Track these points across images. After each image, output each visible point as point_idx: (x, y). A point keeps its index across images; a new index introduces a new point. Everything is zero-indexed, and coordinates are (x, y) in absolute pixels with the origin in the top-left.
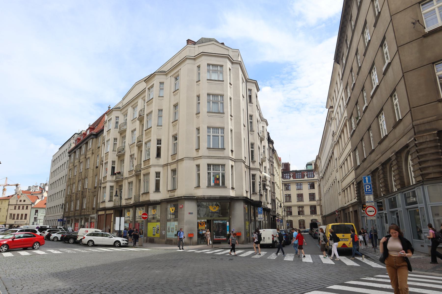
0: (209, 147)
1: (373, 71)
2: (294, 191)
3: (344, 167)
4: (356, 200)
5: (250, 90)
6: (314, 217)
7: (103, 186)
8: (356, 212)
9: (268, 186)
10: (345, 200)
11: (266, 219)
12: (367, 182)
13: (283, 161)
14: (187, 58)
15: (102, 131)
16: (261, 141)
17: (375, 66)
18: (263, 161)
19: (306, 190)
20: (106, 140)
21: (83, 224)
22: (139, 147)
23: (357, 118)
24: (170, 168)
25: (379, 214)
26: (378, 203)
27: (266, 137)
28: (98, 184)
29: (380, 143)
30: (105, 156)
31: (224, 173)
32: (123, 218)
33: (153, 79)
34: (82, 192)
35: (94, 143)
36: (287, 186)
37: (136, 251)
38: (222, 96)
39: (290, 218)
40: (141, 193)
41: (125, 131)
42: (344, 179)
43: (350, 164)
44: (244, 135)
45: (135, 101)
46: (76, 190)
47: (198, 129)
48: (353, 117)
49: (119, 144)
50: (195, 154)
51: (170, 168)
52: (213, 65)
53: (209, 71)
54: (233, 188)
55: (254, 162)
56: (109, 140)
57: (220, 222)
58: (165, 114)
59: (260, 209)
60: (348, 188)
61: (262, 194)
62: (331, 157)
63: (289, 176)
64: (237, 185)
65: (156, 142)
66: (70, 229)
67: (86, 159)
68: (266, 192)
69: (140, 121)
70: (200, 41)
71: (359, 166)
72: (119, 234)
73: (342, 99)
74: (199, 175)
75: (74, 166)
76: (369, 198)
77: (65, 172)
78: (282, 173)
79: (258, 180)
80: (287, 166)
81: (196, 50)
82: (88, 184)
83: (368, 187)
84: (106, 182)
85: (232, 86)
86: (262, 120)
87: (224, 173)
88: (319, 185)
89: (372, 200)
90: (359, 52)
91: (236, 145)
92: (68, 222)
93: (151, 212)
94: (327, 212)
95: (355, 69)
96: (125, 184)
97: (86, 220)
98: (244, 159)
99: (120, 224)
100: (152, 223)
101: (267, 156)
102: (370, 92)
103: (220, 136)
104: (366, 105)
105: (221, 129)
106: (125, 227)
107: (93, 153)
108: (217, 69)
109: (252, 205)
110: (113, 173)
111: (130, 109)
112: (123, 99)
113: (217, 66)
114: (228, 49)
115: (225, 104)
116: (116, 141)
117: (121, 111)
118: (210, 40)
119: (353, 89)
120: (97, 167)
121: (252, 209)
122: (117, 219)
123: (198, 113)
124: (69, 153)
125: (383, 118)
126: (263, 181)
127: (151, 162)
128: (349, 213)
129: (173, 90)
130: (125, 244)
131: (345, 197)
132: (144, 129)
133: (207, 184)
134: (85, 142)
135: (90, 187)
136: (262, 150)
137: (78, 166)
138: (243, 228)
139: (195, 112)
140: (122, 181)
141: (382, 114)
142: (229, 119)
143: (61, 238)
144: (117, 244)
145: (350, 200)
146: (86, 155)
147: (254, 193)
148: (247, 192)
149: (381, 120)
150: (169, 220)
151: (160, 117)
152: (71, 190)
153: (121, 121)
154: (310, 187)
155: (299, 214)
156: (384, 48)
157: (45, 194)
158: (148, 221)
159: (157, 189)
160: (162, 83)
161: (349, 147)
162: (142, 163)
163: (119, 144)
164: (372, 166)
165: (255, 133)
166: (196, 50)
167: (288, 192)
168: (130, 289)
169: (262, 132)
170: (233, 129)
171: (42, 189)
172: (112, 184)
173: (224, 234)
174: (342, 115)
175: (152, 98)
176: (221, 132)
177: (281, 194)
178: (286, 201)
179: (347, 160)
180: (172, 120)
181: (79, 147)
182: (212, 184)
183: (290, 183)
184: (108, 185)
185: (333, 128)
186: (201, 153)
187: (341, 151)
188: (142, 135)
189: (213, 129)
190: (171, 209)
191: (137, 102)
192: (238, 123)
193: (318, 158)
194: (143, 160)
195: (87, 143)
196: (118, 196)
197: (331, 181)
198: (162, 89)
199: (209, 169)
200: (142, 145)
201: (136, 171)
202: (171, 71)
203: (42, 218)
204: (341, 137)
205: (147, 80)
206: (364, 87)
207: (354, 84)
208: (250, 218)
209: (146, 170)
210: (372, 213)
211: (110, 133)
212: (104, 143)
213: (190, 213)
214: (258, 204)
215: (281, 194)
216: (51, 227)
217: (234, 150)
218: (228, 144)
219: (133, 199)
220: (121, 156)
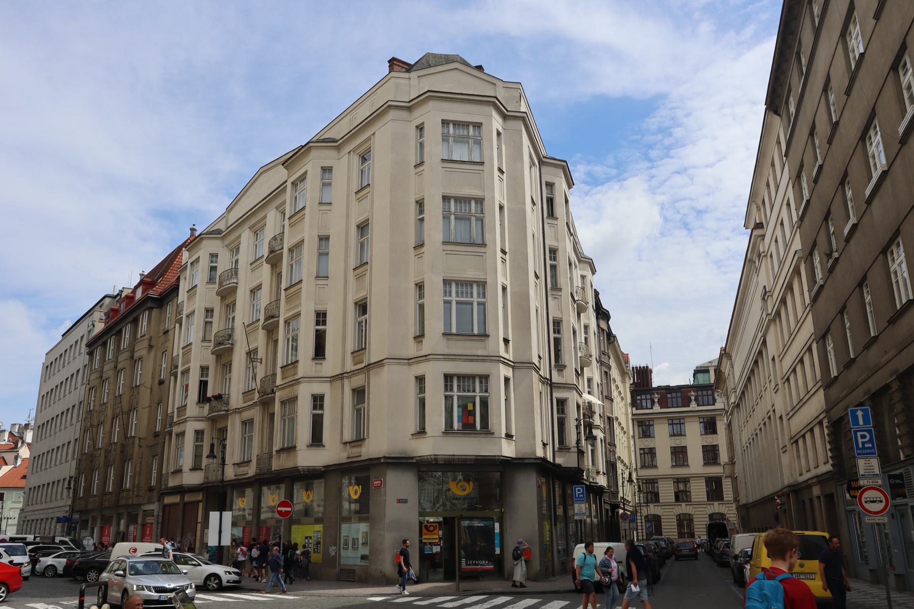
0: (448, 332)
1: (872, 132)
2: (662, 439)
3: (796, 379)
4: (829, 467)
5: (550, 185)
6: (717, 507)
7: (176, 429)
8: (830, 498)
9: (598, 427)
10: (800, 467)
11: (593, 514)
12: (861, 422)
13: (636, 361)
14: (390, 106)
16: (580, 310)
17: (876, 121)
18: (584, 363)
19: (694, 438)
20: (185, 313)
21: (122, 528)
22: (271, 330)
23: (829, 255)
25: (895, 506)
26: (890, 477)
28: (164, 426)
29: (892, 321)
30: (184, 355)
31: (487, 398)
32: (228, 516)
33: (305, 161)
34: (123, 446)
35: (153, 322)
36: (644, 427)
37: (262, 602)
38: (480, 201)
39: (653, 509)
40: (275, 449)
41: (234, 290)
42: (795, 410)
43: (811, 372)
44: (535, 300)
45: (260, 216)
46: (106, 441)
47: (420, 286)
48: (816, 252)
49: (217, 325)
50: (412, 350)
52: (457, 124)
53: (445, 138)
54: (509, 436)
55: (561, 367)
56: (193, 313)
57: (476, 524)
58: (335, 247)
59: (579, 490)
60: (808, 436)
61: (584, 449)
62: (760, 353)
64: (520, 429)
66: (89, 543)
67: (134, 361)
68: (593, 445)
69: (272, 267)
70: (424, 61)
71: (836, 378)
72: (218, 555)
73: (788, 204)
74: (422, 403)
75: (102, 380)
76: (868, 466)
77: (76, 395)
78: (632, 392)
79: (572, 414)
80: (644, 374)
81: (411, 86)
82: (138, 426)
83: (863, 437)
84: (185, 421)
85: (504, 177)
86: (579, 261)
87: (487, 398)
88: (729, 425)
89: (877, 471)
90: (833, 83)
91: (515, 329)
92: (84, 524)
93: (302, 497)
94: (751, 494)
95: (823, 128)
96: (233, 425)
97: (132, 519)
98: (535, 360)
99: (220, 528)
100: (300, 526)
101: (594, 352)
102: (864, 189)
103: (475, 304)
104: (853, 220)
105: (478, 286)
106: (233, 535)
107: (151, 347)
108: (466, 133)
109: (560, 479)
110: (203, 398)
111: (246, 236)
112: (230, 209)
113: (465, 125)
114: (493, 81)
115: (487, 221)
116: (212, 316)
117: (223, 238)
118: (448, 59)
119: (816, 181)
120: (161, 383)
121: (557, 486)
122: (214, 516)
123: (419, 246)
124: (89, 345)
125: (899, 256)
126: (584, 415)
128: (811, 500)
129: (355, 187)
130: (234, 582)
131: (799, 457)
132: (284, 286)
134: (131, 319)
135: (143, 433)
136: (581, 337)
138: (537, 539)
139: (412, 242)
140: (225, 417)
141: (898, 245)
142: (499, 260)
143: (66, 568)
144: (213, 584)
145: (812, 465)
146: (133, 352)
148: (545, 445)
149: (893, 260)
150: (348, 520)
151: (323, 254)
152: (94, 440)
153: (223, 264)
154: (706, 428)
156: (901, 74)
157: (24, 452)
158: (291, 520)
159: (317, 439)
160: (327, 170)
161: (808, 328)
162: (279, 372)
163: (217, 325)
164: (871, 380)
165: (563, 293)
166: (411, 86)
167: (647, 443)
169: (580, 290)
170: (508, 284)
171: (16, 439)
172: (200, 426)
173: (488, 555)
174: (787, 246)
175: (304, 208)
176: (478, 294)
177: (629, 447)
178: (643, 467)
179: (801, 361)
180: (352, 263)
182: (456, 425)
183: (653, 419)
184: (191, 428)
185: (762, 278)
186: (427, 347)
187: (786, 338)
188: (278, 300)
189: (457, 284)
190: (352, 490)
191: (265, 217)
192: (519, 269)
193: (725, 354)
194: (280, 364)
195: (135, 321)
196: (215, 457)
197: (760, 414)
198: (326, 185)
199: (448, 387)
200: (278, 326)
201: (262, 393)
202: (349, 139)
203: (16, 514)
204: (785, 303)
205: (291, 160)
206: (846, 175)
207: (821, 167)
208: (554, 512)
209: (287, 391)
210: (878, 507)
211: (196, 294)
213: (400, 501)
214: (574, 476)
215: (629, 447)
216: (38, 540)
217: (510, 339)
218: (497, 325)
220: (223, 353)
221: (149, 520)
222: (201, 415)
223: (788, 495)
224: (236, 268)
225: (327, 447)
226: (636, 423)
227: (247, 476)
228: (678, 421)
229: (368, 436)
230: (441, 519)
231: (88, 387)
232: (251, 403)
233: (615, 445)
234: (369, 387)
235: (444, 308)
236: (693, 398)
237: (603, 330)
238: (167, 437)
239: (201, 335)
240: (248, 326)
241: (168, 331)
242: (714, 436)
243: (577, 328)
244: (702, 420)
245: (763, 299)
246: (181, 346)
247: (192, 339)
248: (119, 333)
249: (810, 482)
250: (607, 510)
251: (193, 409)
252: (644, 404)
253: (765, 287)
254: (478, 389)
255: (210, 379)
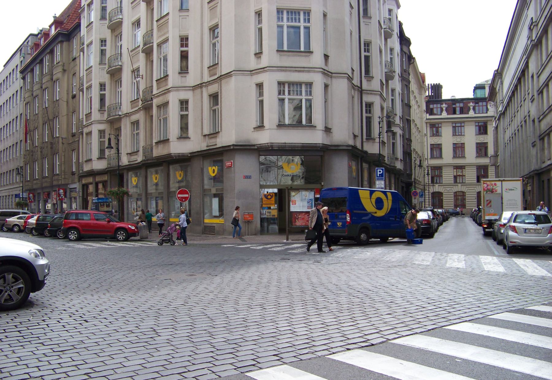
7: (86, 130)
9: (398, 125)
13: (430, 81)
15: (79, 26)
16: (388, 36)
18: (389, 77)
19: (470, 137)
22: (148, 52)
24: (206, 93)
27: (396, 30)
28: (78, 129)
39: (437, 188)
46: (40, 141)
50: (253, 64)
51: (206, 93)
63: (439, 109)
65: (178, 42)
79: (377, 112)
80: (437, 88)
84: (91, 124)
88: (497, 128)
96: (126, 125)
101: (397, 69)
107: (64, 71)
120: (74, 97)
127: (171, 83)
133: (276, 122)
137: (40, 96)
147: (370, 137)
152: (33, 141)
154: (480, 130)
155: (455, 182)
168: (115, 315)
172: (102, 127)
176: (305, 20)
178: (432, 157)
181: (38, 61)
183: (441, 123)
184: (95, 129)
186: (265, 61)
190: (210, 169)
193: (498, 74)
194: (155, 79)
195: (52, 52)
196: (112, 148)
200: (152, 51)
201: (144, 100)
211: (92, 29)
212: (82, 50)
213: (246, 177)
214: (376, 161)
219: (141, 153)
221: (74, 194)
222: (102, 119)
223: (533, 177)
224: (121, 7)
225: (192, 139)
226: (428, 125)
227: (136, 162)
228: (459, 125)
229: (221, 129)
230: (276, 190)
231: (25, 102)
232: (137, 109)
233: (411, 141)
234: (221, 93)
235: (278, 32)
236: (471, 108)
237: (405, 53)
238: (81, 137)
239: (98, 59)
240: (132, 51)
241: (75, 58)
242: (485, 136)
243: (383, 48)
244: (477, 124)
245: (530, 28)
246: (85, 69)
247: (92, 63)
248: (41, 62)
249: (549, 168)
250: (403, 187)
251: (96, 115)
252: (435, 111)
253: (532, 18)
254: (304, 93)
255: (107, 93)
